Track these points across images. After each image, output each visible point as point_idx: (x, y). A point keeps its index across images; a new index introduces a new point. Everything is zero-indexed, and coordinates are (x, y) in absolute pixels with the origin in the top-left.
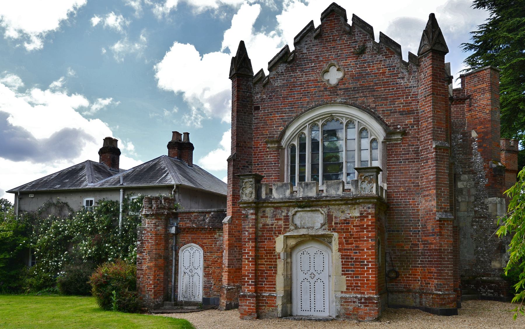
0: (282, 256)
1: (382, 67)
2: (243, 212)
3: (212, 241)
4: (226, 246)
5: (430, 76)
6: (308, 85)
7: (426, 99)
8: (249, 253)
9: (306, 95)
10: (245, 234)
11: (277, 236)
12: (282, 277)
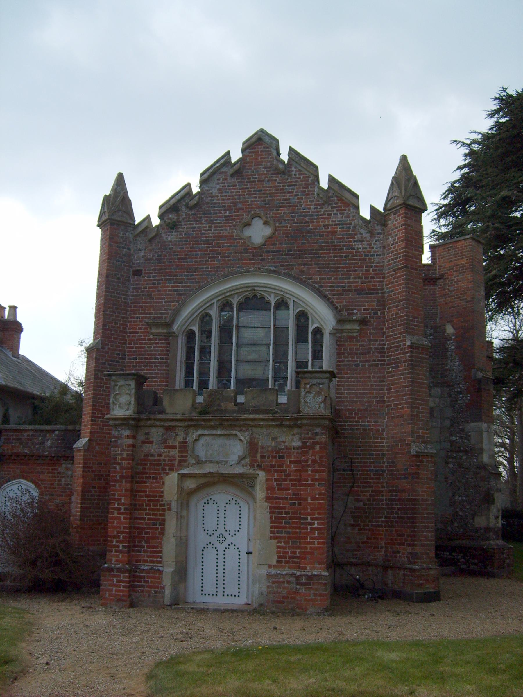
0: (174, 505)
1: (331, 223)
2: (115, 433)
3: (55, 477)
4: (78, 488)
5: (402, 241)
6: (219, 243)
7: (396, 274)
8: (120, 500)
9: (215, 257)
10: (115, 468)
11: (167, 474)
12: (173, 541)
